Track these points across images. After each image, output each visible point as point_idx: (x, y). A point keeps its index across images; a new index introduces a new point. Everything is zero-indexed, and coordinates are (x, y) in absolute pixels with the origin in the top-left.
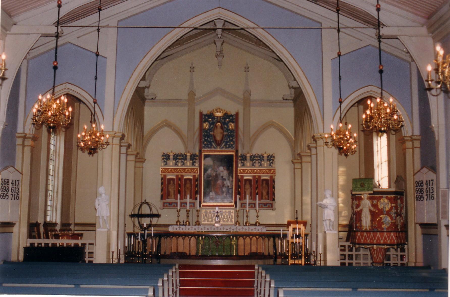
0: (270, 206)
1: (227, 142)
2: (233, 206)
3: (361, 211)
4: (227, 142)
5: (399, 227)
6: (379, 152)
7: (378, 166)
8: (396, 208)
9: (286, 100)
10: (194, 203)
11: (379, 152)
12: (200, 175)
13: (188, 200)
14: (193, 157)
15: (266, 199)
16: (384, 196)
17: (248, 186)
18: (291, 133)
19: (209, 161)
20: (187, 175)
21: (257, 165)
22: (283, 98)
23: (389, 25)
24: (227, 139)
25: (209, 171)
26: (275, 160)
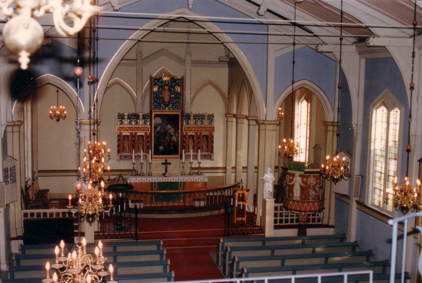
0: (210, 157)
1: (174, 103)
2: (178, 158)
3: (294, 185)
4: (174, 103)
5: (320, 197)
6: (299, 115)
7: (298, 126)
8: (320, 183)
9: (222, 61)
10: (146, 156)
11: (299, 115)
12: (151, 133)
13: (142, 154)
14: (144, 117)
15: (206, 152)
16: (312, 175)
17: (191, 141)
18: (225, 90)
19: (158, 120)
20: (139, 133)
21: (199, 123)
22: (219, 60)
23: (327, 43)
24: (174, 101)
25: (159, 129)
26: (214, 119)
